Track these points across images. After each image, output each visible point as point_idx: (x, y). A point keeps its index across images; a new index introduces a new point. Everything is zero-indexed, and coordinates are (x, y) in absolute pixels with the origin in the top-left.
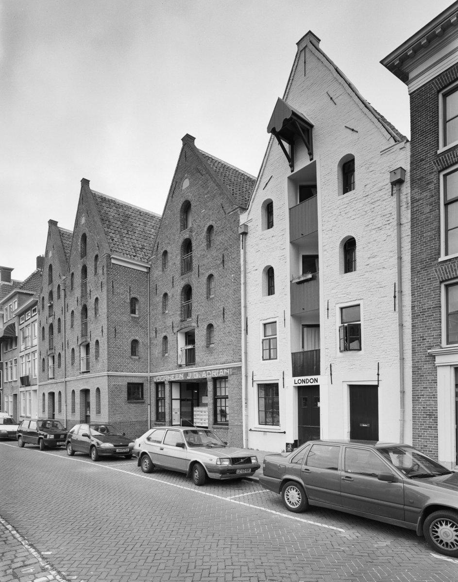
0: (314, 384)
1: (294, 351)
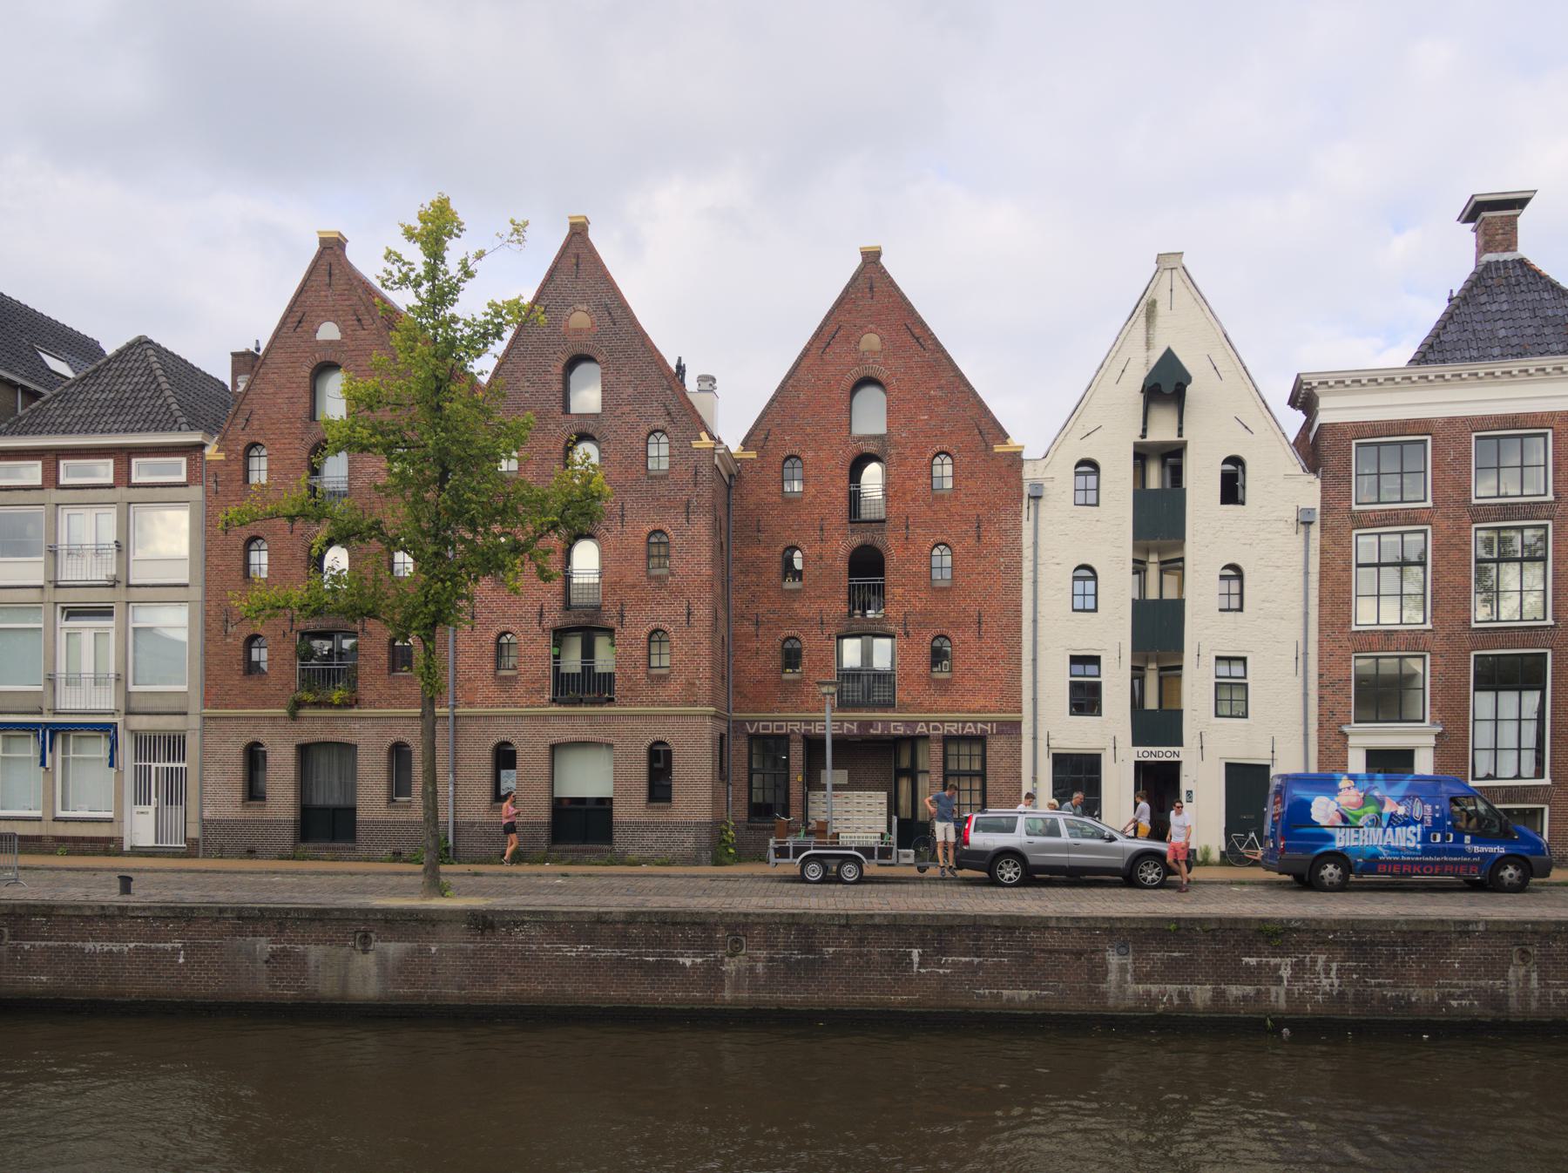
0: (1172, 759)
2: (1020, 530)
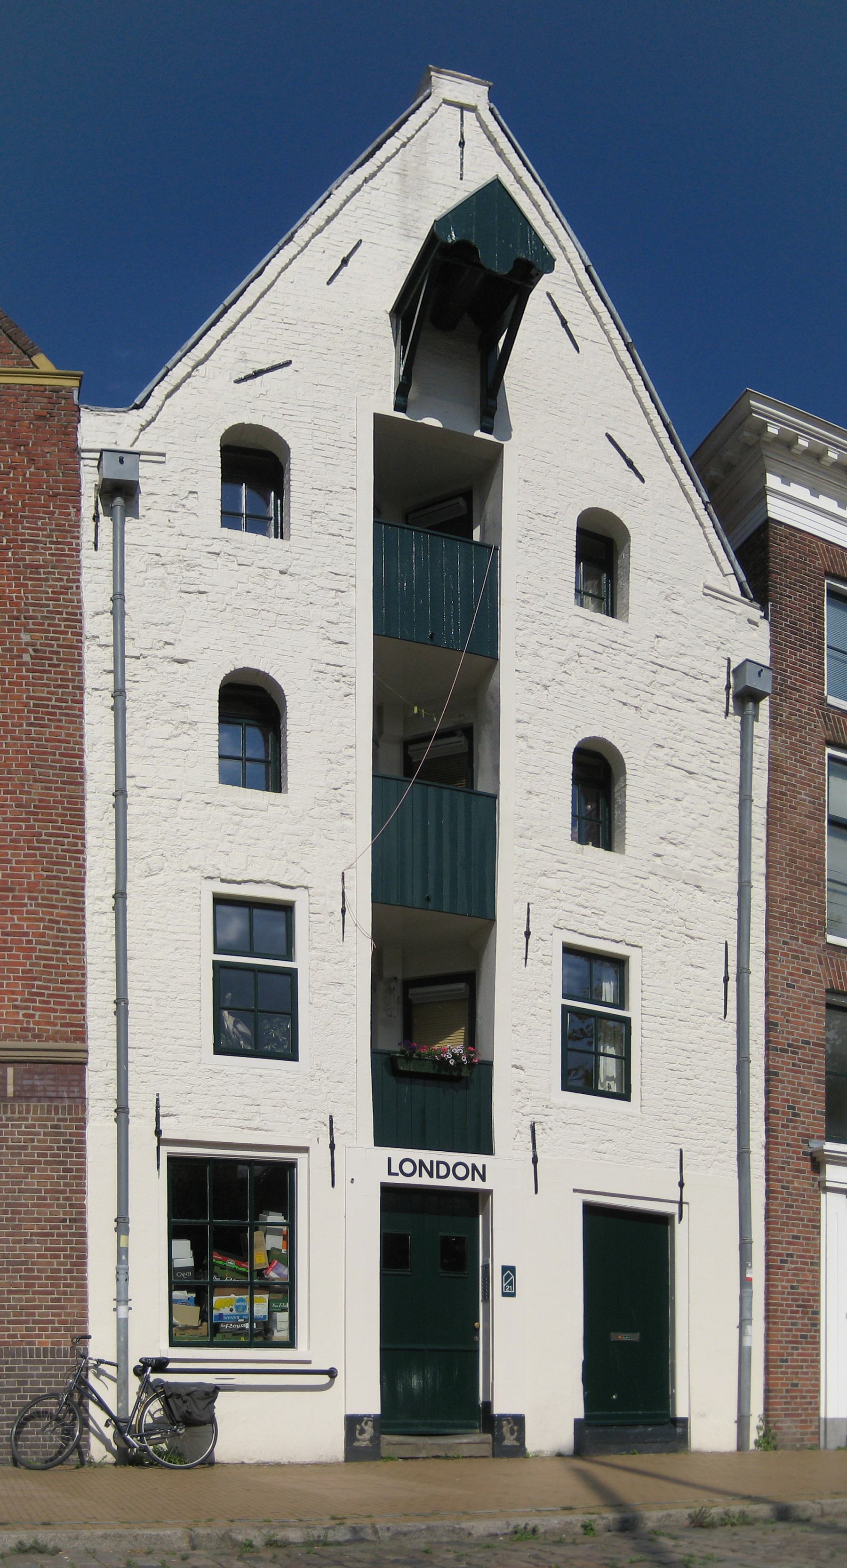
0: (468, 1184)
2: (77, 569)
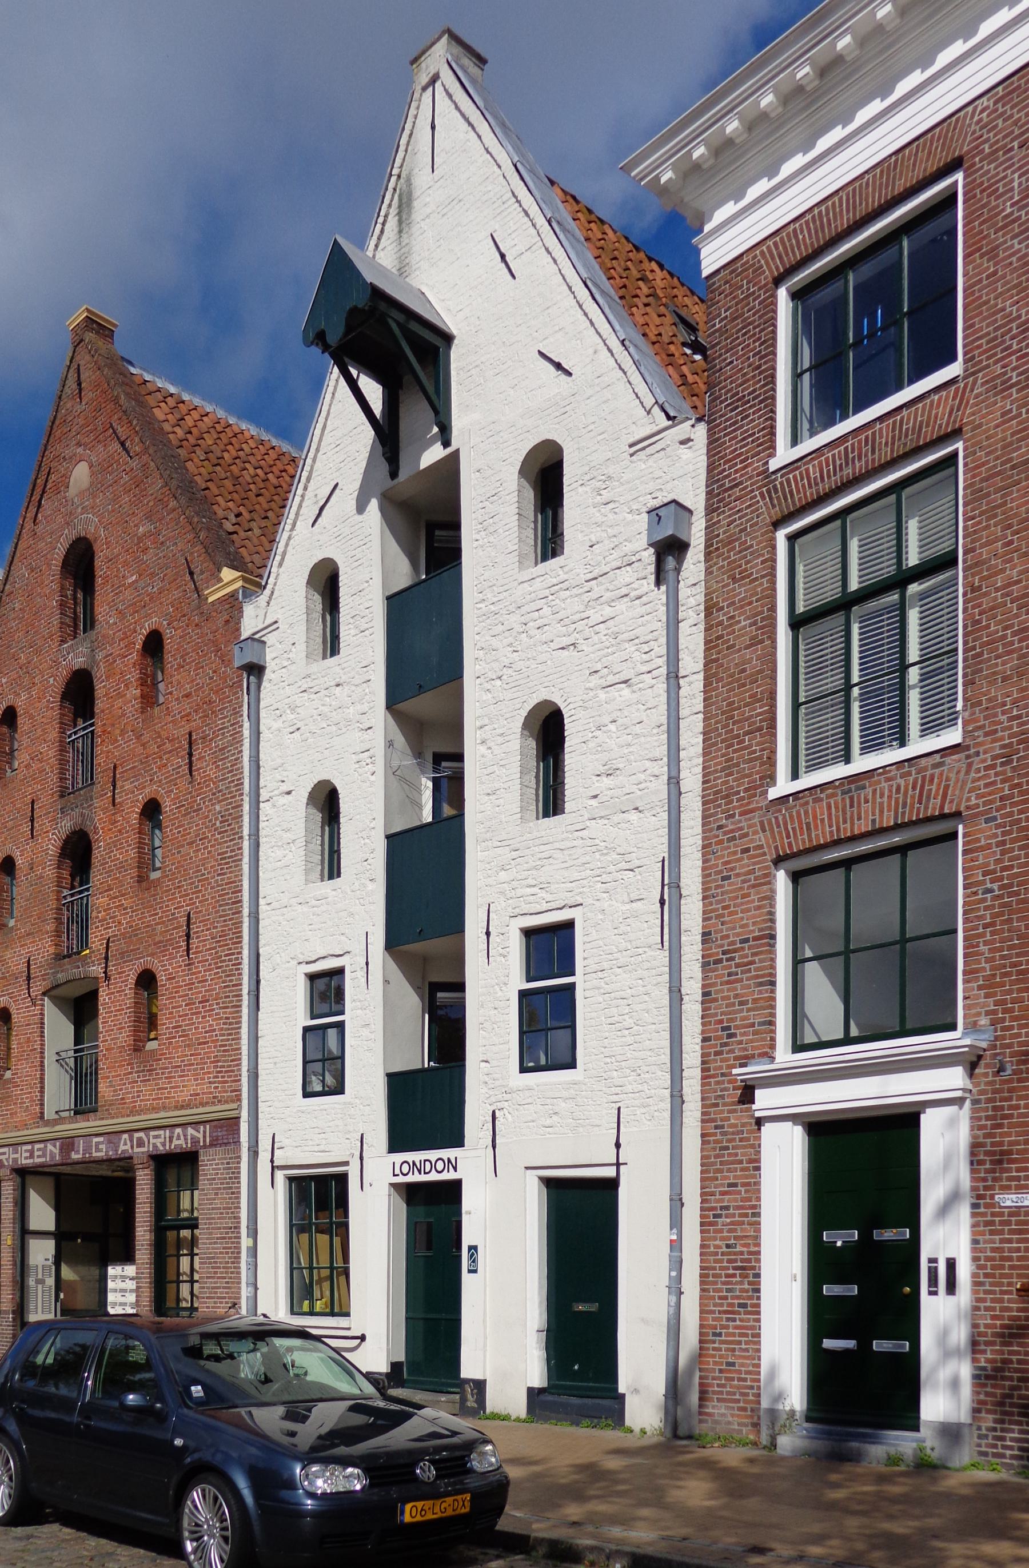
1: (399, 1066)
